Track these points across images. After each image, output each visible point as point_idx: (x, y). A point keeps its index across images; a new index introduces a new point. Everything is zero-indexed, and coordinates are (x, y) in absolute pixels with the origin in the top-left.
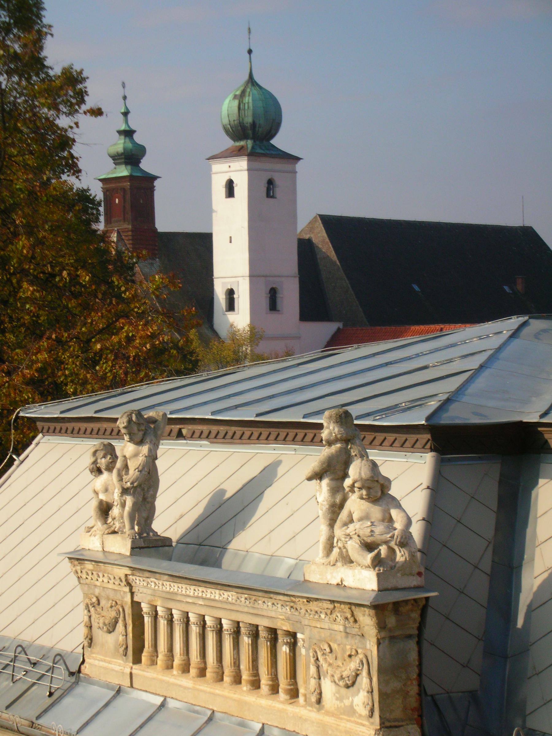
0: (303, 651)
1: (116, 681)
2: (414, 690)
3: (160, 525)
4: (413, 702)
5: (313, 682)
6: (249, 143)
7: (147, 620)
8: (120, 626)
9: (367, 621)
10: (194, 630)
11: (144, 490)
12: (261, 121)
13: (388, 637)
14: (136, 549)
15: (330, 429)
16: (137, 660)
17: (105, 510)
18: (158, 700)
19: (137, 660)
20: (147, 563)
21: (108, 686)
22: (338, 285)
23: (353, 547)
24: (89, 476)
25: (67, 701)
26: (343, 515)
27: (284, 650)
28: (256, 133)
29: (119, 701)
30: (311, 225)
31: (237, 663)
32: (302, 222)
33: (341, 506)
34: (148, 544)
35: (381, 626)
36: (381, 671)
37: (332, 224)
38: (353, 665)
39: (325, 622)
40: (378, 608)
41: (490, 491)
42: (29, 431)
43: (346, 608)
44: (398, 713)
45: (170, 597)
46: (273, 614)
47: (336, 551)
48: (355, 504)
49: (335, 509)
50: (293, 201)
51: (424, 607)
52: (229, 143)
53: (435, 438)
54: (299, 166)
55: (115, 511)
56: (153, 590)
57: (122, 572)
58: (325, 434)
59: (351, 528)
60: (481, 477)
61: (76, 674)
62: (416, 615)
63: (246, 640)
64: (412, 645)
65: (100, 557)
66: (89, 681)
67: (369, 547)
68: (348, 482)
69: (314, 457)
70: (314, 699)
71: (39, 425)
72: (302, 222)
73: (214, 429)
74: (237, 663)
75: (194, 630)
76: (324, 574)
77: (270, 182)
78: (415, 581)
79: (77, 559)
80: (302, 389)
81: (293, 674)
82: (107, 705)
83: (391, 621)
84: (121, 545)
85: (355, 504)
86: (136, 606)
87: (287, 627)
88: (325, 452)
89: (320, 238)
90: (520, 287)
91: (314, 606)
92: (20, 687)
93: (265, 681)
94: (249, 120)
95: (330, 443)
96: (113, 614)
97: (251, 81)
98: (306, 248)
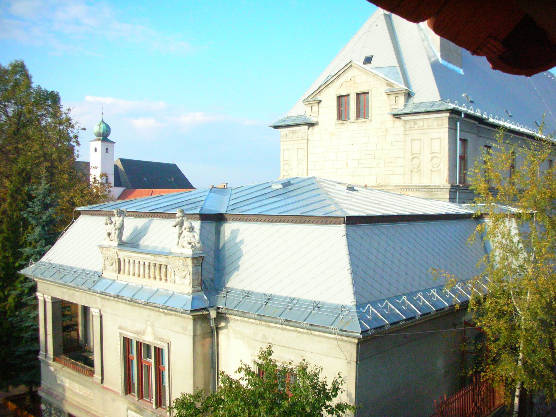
0: (170, 270)
1: (113, 278)
2: (200, 278)
3: (124, 238)
4: (200, 281)
5: (173, 277)
6: (102, 138)
7: (122, 263)
8: (114, 264)
9: (190, 262)
10: (137, 265)
11: (121, 229)
12: (105, 132)
13: (195, 266)
14: (119, 245)
15: (179, 214)
16: (119, 272)
17: (109, 234)
18: (126, 283)
19: (119, 272)
20: (122, 248)
21: (110, 280)
22: (124, 177)
23: (185, 244)
24: (104, 225)
25: (99, 283)
26: (182, 236)
27: (163, 270)
28: (104, 136)
29: (114, 283)
30: (117, 161)
31: (149, 273)
32: (115, 160)
33: (181, 233)
34: (122, 244)
35: (193, 263)
36: (193, 274)
37: (123, 161)
38: (185, 272)
39: (177, 262)
40: (193, 258)
41: (213, 230)
42: (79, 214)
43: (183, 258)
44: (196, 284)
45: (130, 257)
46: (162, 260)
47: (180, 245)
48: (186, 233)
49: (180, 234)
50: (113, 154)
51: (203, 258)
52: (96, 138)
53: (200, 217)
54: (115, 145)
55: (112, 235)
56: (125, 255)
57: (115, 250)
58: (177, 215)
59: (185, 239)
60: (211, 226)
61: (100, 276)
62: (201, 260)
63: (152, 267)
64: (200, 267)
65: (108, 246)
66: (104, 278)
67: (190, 243)
68: (184, 227)
69: (173, 222)
70: (173, 281)
71: (81, 212)
72: (115, 160)
73: (136, 214)
74: (149, 273)
75: (137, 265)
76: (176, 250)
77: (107, 149)
78: (201, 252)
79: (101, 247)
80: (158, 204)
81: (166, 276)
82: (111, 284)
83: (196, 262)
84: (115, 243)
85: (186, 233)
86: (119, 259)
87: (165, 264)
88: (177, 220)
89: (120, 165)
90: (172, 180)
91: (174, 258)
92: (84, 281)
93: (158, 277)
94: (102, 132)
95: (178, 218)
96: (112, 261)
97: (103, 121)
98: (116, 167)
